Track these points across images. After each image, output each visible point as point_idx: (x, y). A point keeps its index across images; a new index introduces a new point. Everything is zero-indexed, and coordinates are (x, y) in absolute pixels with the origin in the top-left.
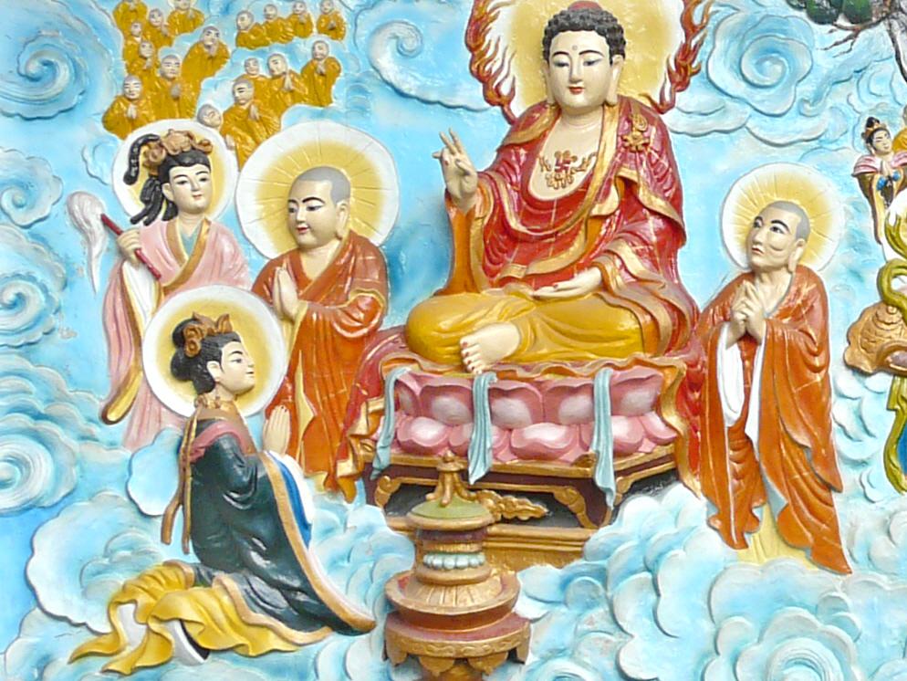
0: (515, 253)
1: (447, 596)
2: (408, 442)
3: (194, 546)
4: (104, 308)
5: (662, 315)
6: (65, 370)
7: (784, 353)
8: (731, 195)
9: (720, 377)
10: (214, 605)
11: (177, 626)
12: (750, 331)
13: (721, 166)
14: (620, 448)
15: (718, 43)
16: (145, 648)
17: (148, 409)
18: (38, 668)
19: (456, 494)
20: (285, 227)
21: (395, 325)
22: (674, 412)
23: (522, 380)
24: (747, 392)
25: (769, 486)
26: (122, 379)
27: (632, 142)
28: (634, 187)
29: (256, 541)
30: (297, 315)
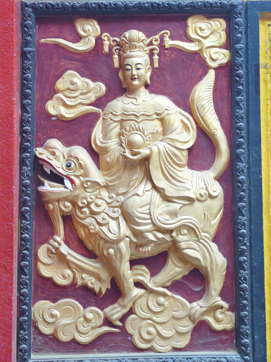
2: (137, 279)
4: (48, 359)
7: (269, 159)
8: (140, 355)
9: (150, 169)
10: (158, 201)
11: (103, 213)
14: (217, 178)
18: (247, 88)
20: (209, 283)
21: (262, 71)
22: (193, 233)
24: (211, 249)
25: (43, 181)
26: (170, 199)
27: (11, 45)
28: (150, 92)
29: (166, 166)
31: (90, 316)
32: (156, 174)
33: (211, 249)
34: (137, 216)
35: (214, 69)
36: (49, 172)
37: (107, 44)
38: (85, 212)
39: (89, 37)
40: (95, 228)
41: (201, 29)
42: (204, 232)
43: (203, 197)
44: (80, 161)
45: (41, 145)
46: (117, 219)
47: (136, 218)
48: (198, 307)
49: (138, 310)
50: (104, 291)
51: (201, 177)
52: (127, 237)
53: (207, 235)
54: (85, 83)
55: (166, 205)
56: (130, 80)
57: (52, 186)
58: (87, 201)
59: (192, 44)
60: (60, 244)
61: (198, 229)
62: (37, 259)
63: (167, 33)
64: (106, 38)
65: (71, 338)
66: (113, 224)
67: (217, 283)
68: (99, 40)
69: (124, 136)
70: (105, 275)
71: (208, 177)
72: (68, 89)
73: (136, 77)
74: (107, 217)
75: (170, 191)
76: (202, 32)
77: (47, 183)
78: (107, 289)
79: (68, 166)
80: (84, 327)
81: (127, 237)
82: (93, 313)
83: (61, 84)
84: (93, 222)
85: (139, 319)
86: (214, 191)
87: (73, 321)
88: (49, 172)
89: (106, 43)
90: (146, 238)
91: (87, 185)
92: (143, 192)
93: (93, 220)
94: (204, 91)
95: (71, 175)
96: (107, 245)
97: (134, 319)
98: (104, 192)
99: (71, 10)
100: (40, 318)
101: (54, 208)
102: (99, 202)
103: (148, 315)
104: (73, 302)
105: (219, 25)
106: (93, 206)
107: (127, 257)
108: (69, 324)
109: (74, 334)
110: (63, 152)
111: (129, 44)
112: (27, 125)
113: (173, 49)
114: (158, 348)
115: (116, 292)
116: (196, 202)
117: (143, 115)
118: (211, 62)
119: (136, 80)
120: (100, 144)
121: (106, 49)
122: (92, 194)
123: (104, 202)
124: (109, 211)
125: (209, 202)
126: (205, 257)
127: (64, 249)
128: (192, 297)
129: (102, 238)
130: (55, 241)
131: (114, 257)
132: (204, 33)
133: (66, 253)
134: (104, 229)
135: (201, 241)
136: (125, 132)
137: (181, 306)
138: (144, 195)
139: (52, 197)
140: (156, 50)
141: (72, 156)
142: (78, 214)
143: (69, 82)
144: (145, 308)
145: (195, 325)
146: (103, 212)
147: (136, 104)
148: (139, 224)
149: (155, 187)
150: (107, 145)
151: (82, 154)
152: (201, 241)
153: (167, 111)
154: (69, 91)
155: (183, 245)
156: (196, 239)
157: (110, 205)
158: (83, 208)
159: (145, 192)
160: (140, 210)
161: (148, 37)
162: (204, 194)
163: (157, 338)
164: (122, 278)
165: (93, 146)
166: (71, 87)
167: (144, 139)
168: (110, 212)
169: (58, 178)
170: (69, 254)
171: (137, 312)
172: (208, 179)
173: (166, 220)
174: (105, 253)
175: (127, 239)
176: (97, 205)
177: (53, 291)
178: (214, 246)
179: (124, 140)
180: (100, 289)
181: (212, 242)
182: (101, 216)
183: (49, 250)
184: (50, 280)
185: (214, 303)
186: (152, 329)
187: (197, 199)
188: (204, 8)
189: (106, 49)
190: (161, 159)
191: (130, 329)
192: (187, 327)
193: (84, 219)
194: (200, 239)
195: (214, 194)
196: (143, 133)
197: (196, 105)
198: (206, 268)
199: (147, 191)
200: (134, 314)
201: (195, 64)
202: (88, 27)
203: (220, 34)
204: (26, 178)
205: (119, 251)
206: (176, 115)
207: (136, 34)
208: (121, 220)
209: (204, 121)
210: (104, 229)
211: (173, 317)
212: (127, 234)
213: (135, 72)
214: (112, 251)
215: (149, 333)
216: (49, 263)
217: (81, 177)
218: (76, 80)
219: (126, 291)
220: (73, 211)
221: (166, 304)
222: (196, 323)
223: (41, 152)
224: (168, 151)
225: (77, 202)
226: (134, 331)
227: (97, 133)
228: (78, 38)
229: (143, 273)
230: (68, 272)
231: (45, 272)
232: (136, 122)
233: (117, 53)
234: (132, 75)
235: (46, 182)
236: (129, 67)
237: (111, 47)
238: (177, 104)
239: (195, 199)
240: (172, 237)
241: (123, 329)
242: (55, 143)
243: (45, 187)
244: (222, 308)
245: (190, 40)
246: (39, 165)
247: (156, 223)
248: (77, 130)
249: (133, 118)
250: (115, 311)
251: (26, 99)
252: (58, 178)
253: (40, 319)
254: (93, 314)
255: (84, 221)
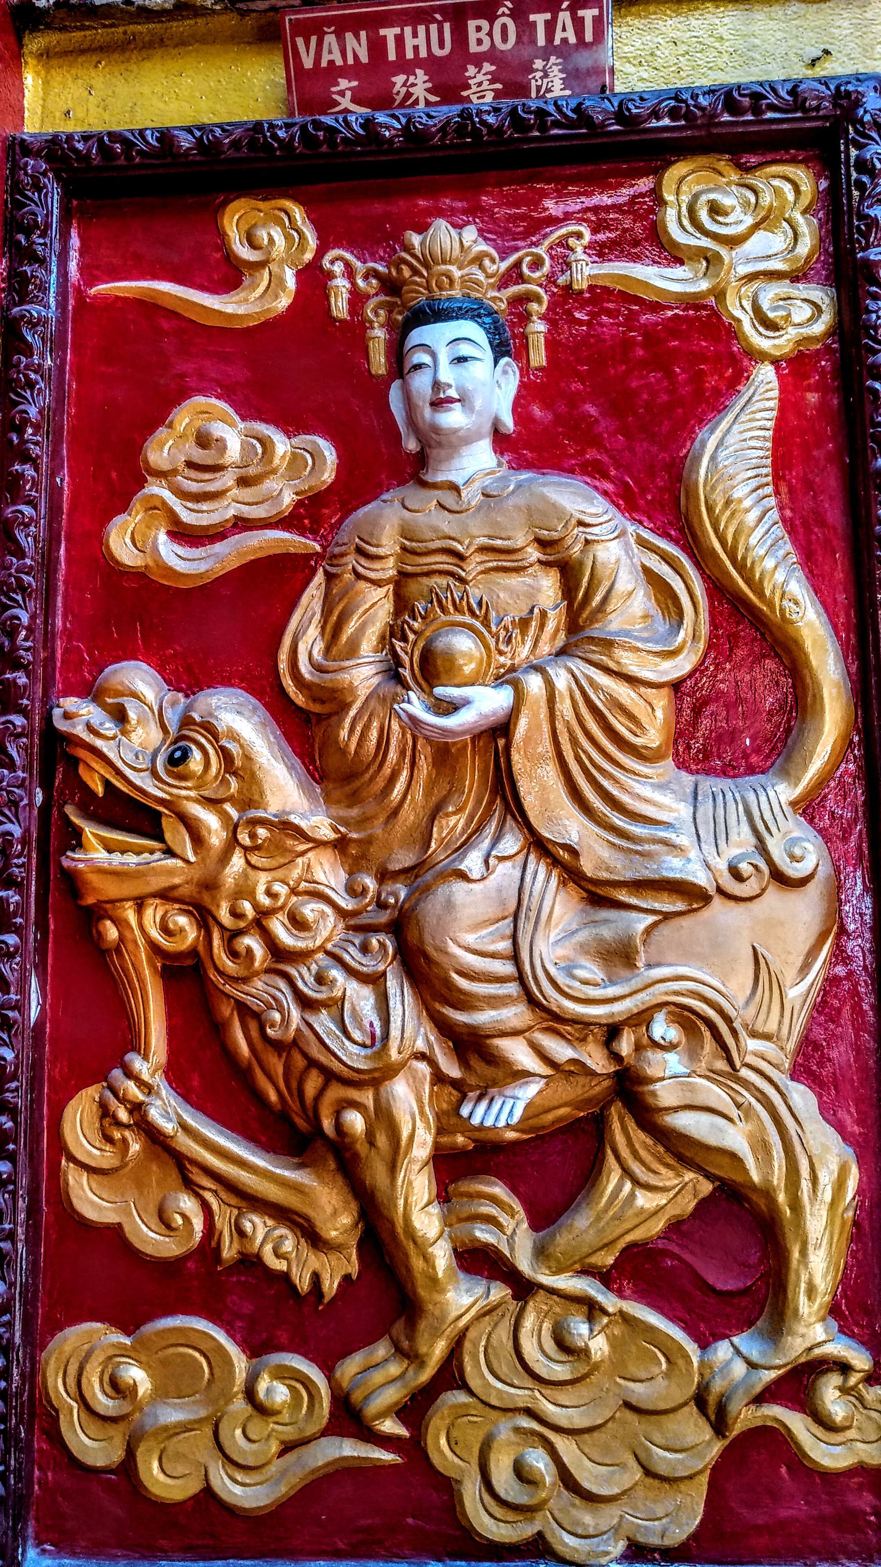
0: (30, 1531)
1: (761, 453)
3: (746, 1171)
5: (189, 1204)
6: (805, 275)
12: (773, 1346)
13: (451, 824)
15: (289, 1427)
16: (668, 845)
17: (605, 1537)
19: (509, 817)
23: (524, 248)
24: (789, 1108)
30: (538, 864)
31: (278, 1393)
32: (540, 785)
33: (789, 1108)
34: (459, 964)
35: (775, 362)
36: (100, 790)
37: (344, 290)
38: (249, 950)
39: (274, 267)
40: (286, 1021)
41: (715, 210)
42: (754, 1035)
43: (747, 883)
44: (224, 742)
45: (89, 690)
46: (375, 980)
47: (455, 976)
48: (739, 1369)
49: (475, 1370)
50: (330, 1286)
51: (735, 801)
52: (421, 1056)
53: (766, 1054)
54: (254, 437)
55: (590, 919)
56: (427, 412)
57: (112, 846)
58: (256, 906)
59: (680, 272)
60: (148, 1089)
61: (728, 1020)
62: (59, 1147)
63: (579, 236)
64: (338, 268)
65: (193, 1487)
66: (361, 999)
67: (818, 1265)
68: (313, 279)
69: (404, 639)
70: (337, 1218)
71: (763, 799)
72: (190, 465)
73: (452, 393)
74: (336, 974)
75: (598, 855)
76: (720, 219)
77: (96, 836)
78: (347, 1278)
79: (177, 761)
80: (249, 1440)
81: (421, 1056)
82: (287, 1382)
83: (164, 449)
84: (279, 994)
85: (480, 1406)
86: (793, 858)
87: (203, 1413)
88: (100, 790)
89: (341, 284)
90: (494, 1059)
91: (253, 836)
92: (486, 862)
93: (282, 984)
94: (736, 454)
95: (187, 798)
96: (336, 1092)
97: (461, 1411)
98: (327, 867)
99: (198, 158)
100: (68, 1394)
101: (122, 938)
102: (310, 910)
103: (521, 1396)
104: (204, 1333)
105: (790, 186)
106: (279, 928)
107: (422, 1147)
108: (186, 1427)
109: (206, 1471)
110: (161, 707)
111: (426, 274)
112: (17, 601)
113: (599, 295)
114: (566, 1545)
115: (386, 1290)
116: (717, 901)
117: (483, 549)
118: (761, 334)
119: (450, 410)
120: (311, 673)
121: (340, 307)
122: (279, 874)
123: (328, 910)
124: (345, 944)
125: (775, 900)
126: (761, 1147)
127: (167, 1111)
128: (710, 1317)
129: (312, 1063)
130: (130, 1074)
131: (362, 1148)
132: (726, 224)
133: (168, 1127)
134: (323, 1022)
135: (745, 1073)
136: (411, 622)
137: (663, 1360)
138: (492, 877)
139: (111, 889)
140: (538, 299)
141: (194, 723)
142: (220, 958)
143: (192, 440)
144: (506, 1364)
145: (727, 1442)
146: (322, 948)
147: (457, 508)
148: (465, 1002)
149: (538, 844)
150: (340, 676)
151: (237, 716)
152: (745, 1073)
153: (581, 529)
154: (193, 474)
155: (665, 1094)
156: (721, 1065)
157: (352, 922)
158: (239, 933)
159: (492, 861)
160: (470, 939)
161: (504, 254)
162: (751, 868)
163: (561, 1501)
164: (402, 1236)
165: (288, 683)
166: (199, 455)
167: (487, 647)
168: (351, 949)
169: (135, 816)
170: (184, 1127)
171: (474, 1383)
172: (765, 806)
173: (585, 982)
174: (327, 1124)
175: (423, 1067)
176: (298, 923)
177: (127, 1286)
178: (803, 1098)
179: (406, 653)
180: (316, 1278)
181: (792, 1079)
182: (314, 967)
183: (105, 1112)
184: (114, 1234)
185: (810, 1349)
186: (539, 1461)
187: (720, 891)
188: (726, 118)
189: (340, 307)
190: (559, 726)
191: (441, 1452)
192: (695, 1446)
193: (245, 980)
194: (738, 1064)
195: (795, 871)
196: (482, 623)
197: (706, 502)
198: (768, 1193)
199: (502, 859)
200: (459, 1388)
201: (698, 355)
202: (275, 236)
203: (792, 227)
204: (8, 813)
205: (383, 1117)
206: (618, 548)
207: (455, 245)
208: (394, 984)
209: (741, 567)
210: (323, 1022)
211: (628, 1405)
212: (420, 1045)
213: (446, 373)
214: (356, 1121)
215: (521, 1472)
216: (105, 1165)
217: (228, 807)
218: (219, 429)
219: (422, 1293)
220: (201, 949)
221: (599, 1346)
222: (731, 1438)
223: (80, 715)
224: (584, 682)
225: (213, 909)
226: (461, 1463)
227: (304, 638)
228: (229, 275)
229: (493, 1210)
230: (187, 1203)
231: (91, 1201)
232: (456, 579)
233: (382, 319)
234: (437, 385)
235: (90, 830)
236: (426, 359)
237: (357, 299)
238: (628, 501)
239: (712, 891)
240: (616, 1057)
241: (414, 1448)
242: (140, 680)
243: (86, 851)
244: (845, 1368)
245: (674, 255)
246: (58, 754)
247: (541, 992)
248: (222, 630)
249: (441, 561)
250: (378, 1377)
251: (14, 503)
252: (135, 816)
253: (69, 1400)
254: (289, 1387)
255: (246, 988)
